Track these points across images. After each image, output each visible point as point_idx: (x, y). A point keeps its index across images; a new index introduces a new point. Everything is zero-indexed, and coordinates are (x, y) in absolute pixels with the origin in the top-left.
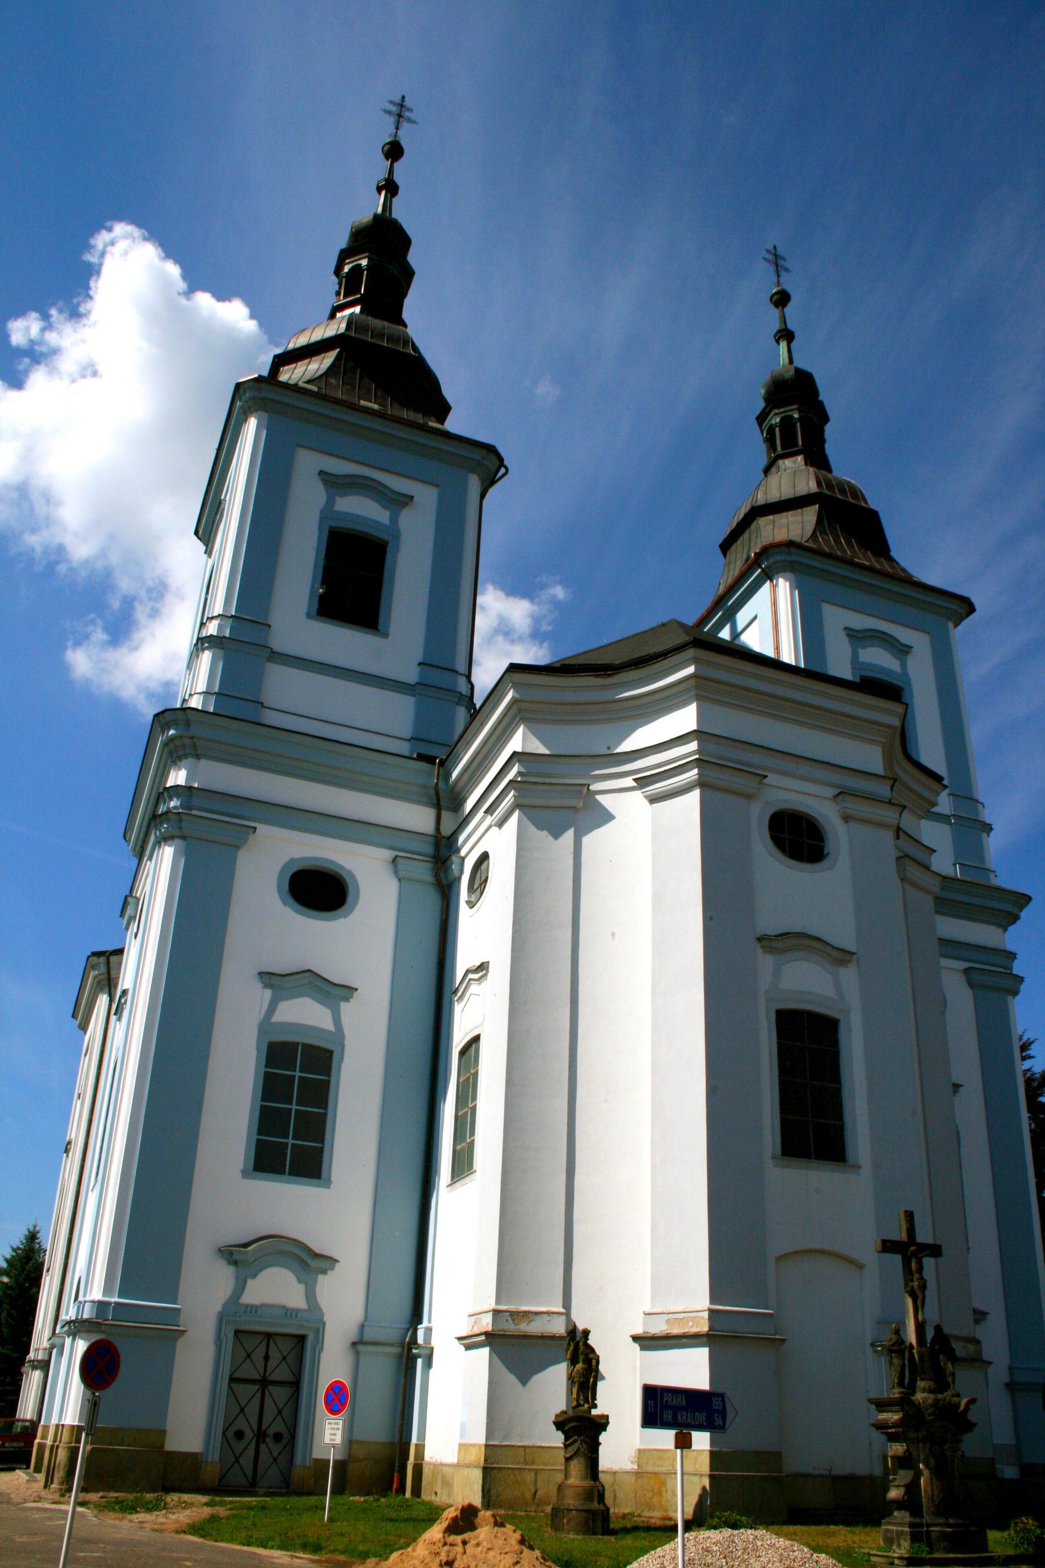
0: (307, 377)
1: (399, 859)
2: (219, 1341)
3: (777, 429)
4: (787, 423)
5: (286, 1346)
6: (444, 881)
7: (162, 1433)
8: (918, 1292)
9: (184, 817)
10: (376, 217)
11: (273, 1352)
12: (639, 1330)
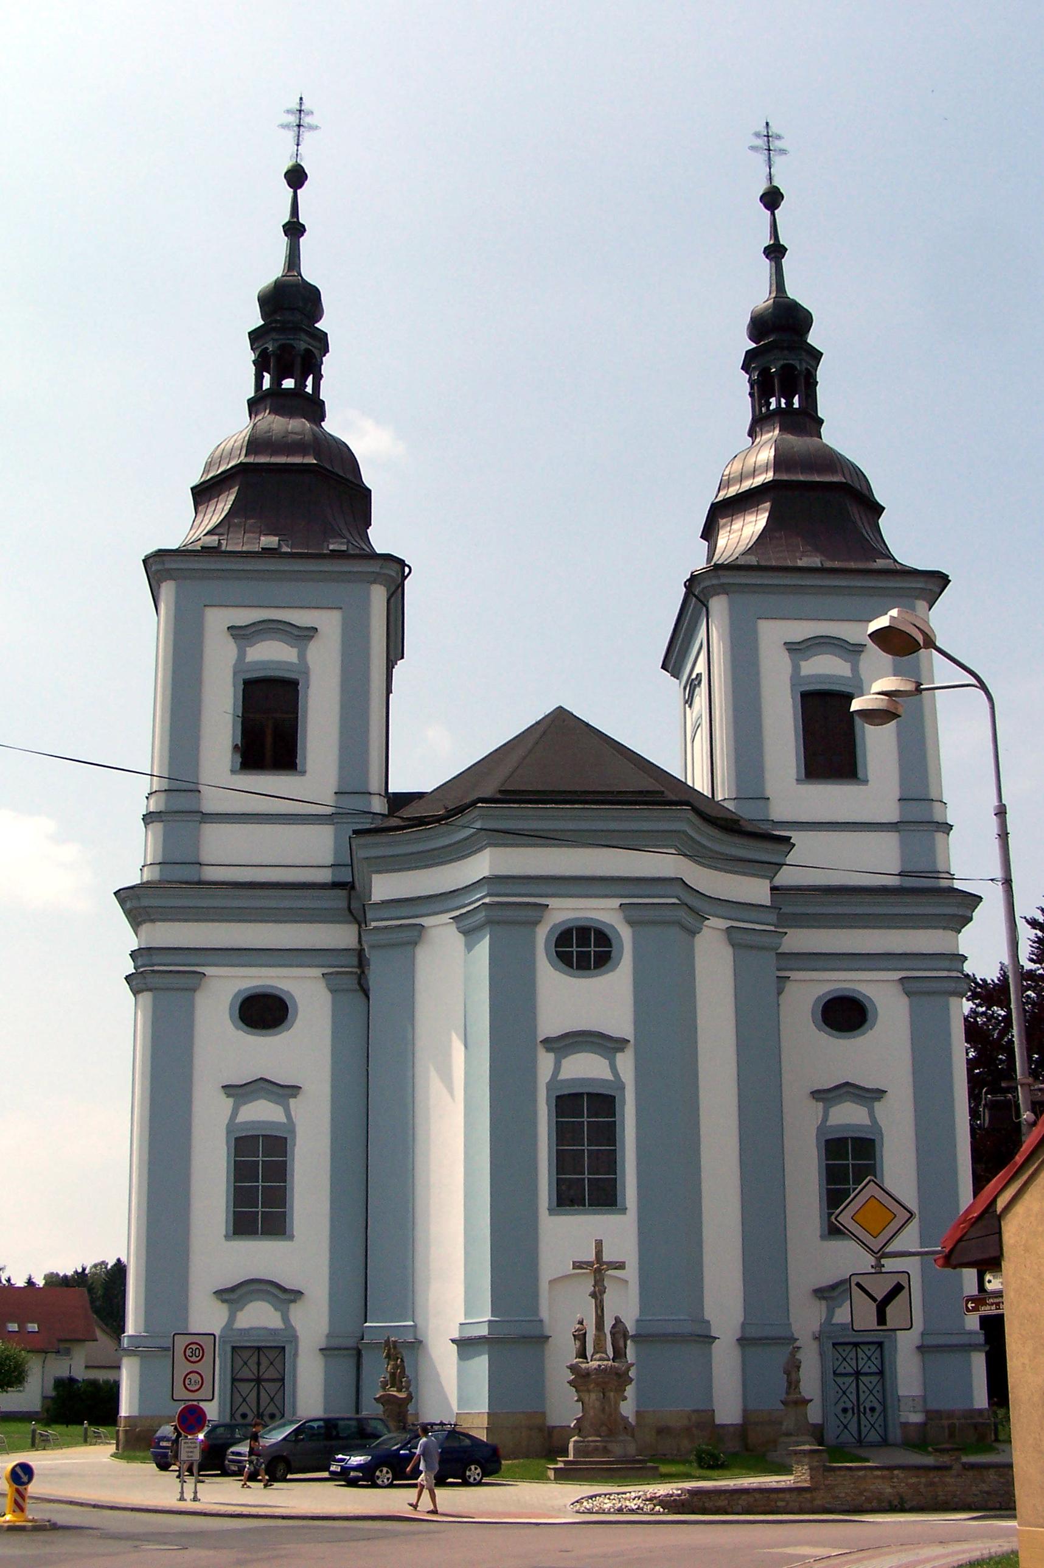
7: (544, 1414)
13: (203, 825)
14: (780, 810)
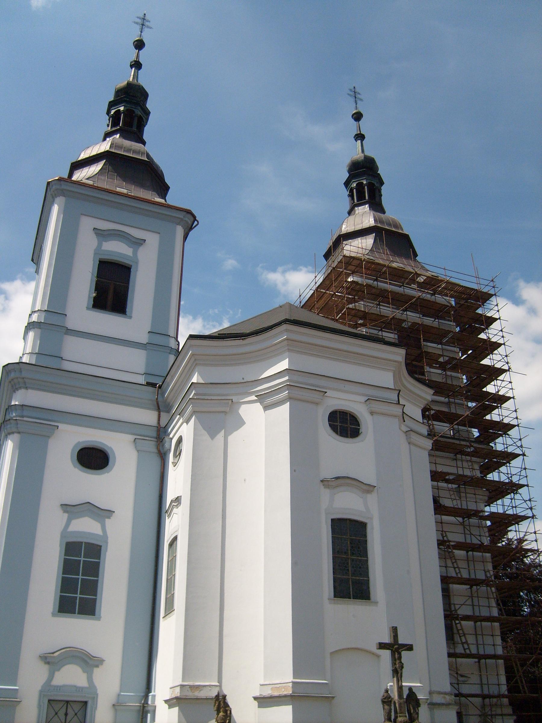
0: (86, 177)
1: (137, 440)
2: (39, 706)
3: (355, 190)
4: (360, 186)
5: (77, 707)
6: (162, 451)
8: (399, 670)
9: (18, 422)
10: (129, 85)
11: (70, 711)
12: (257, 694)
13: (65, 336)
14: (72, 323)
